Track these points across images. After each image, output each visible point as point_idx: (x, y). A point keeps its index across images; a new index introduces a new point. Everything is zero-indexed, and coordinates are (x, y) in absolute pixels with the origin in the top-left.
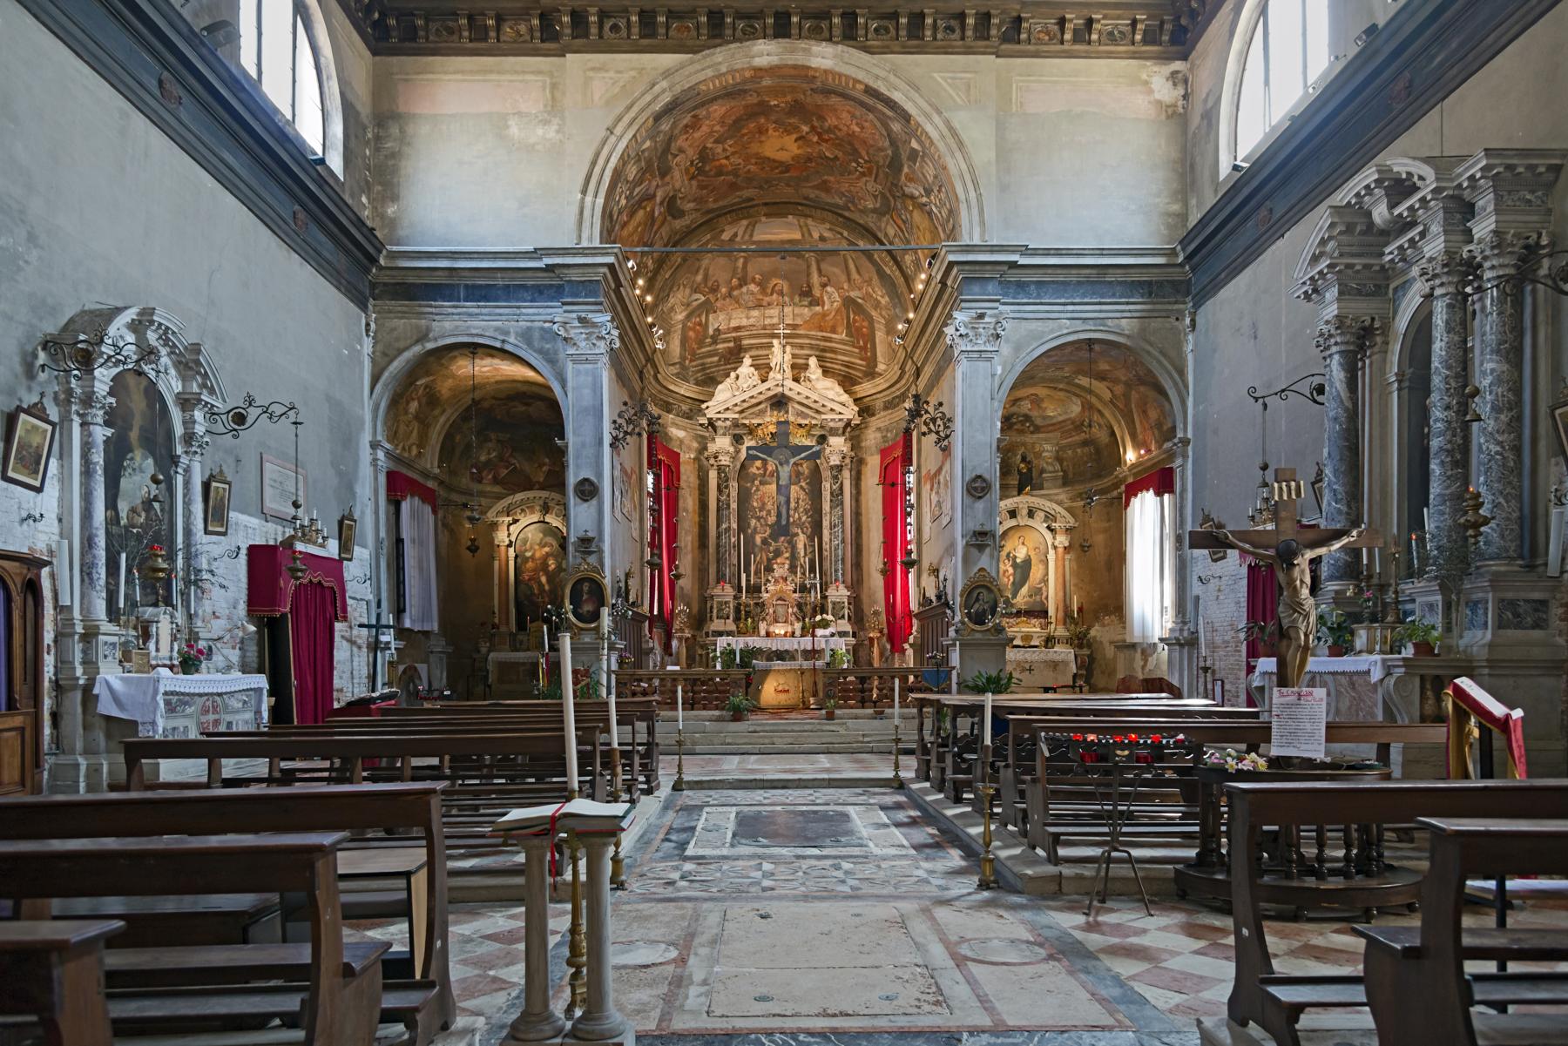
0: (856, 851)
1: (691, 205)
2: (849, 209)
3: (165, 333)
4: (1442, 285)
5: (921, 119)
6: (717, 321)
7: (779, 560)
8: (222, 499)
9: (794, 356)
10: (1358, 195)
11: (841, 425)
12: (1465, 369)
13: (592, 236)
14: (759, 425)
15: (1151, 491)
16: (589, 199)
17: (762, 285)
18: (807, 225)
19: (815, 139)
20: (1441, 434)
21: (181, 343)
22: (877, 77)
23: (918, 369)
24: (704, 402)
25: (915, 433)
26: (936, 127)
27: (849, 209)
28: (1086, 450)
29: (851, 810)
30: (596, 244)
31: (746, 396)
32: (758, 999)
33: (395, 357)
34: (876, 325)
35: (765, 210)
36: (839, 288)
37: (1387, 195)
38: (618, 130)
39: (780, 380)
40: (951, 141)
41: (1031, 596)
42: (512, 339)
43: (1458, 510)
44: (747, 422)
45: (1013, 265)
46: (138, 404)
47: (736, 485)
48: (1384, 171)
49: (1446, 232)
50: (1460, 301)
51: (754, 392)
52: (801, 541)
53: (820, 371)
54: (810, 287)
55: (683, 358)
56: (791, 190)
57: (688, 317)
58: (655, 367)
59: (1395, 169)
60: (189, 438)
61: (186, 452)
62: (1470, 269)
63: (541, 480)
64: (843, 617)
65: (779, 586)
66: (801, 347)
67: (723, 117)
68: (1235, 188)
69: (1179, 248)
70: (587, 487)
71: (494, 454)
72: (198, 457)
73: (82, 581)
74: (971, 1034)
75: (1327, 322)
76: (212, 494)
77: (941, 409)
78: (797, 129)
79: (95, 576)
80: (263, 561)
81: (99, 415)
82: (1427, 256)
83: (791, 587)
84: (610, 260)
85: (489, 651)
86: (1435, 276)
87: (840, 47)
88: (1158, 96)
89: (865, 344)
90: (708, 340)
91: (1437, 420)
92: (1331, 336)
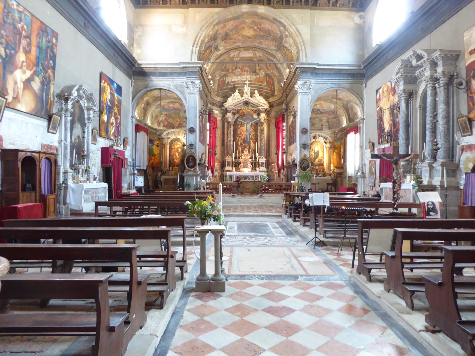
0: (271, 235)
1: (222, 48)
2: (267, 49)
3: (85, 91)
4: (429, 84)
5: (289, 27)
6: (229, 79)
7: (245, 149)
8: (96, 135)
9: (251, 90)
10: (408, 57)
11: (264, 110)
12: (435, 107)
13: (195, 59)
14: (240, 110)
15: (353, 132)
16: (194, 48)
17: (242, 69)
18: (255, 53)
19: (259, 30)
20: (429, 124)
21: (88, 93)
22: (277, 15)
23: (287, 95)
24: (224, 103)
25: (286, 115)
26: (293, 29)
27: (267, 49)
28: (335, 119)
29: (268, 223)
30: (196, 61)
31: (236, 101)
32: (250, 268)
33: (139, 92)
34: (275, 81)
35: (243, 49)
36: (264, 71)
37: (416, 58)
38: (203, 29)
39: (247, 97)
40: (297, 33)
41: (319, 162)
42: (172, 87)
43: (433, 145)
44: (236, 109)
45: (315, 68)
46: (77, 110)
47: (233, 127)
48: (415, 52)
49: (430, 70)
50: (434, 88)
51: (239, 100)
52: (252, 143)
53: (258, 94)
54: (256, 70)
55: (218, 90)
56: (251, 44)
57: (220, 78)
58: (210, 93)
59: (417, 52)
60: (89, 118)
61: (88, 122)
62: (436, 80)
63: (177, 126)
64: (264, 166)
65: (246, 157)
66: (253, 87)
67: (232, 25)
68: (377, 50)
69: (362, 65)
70: (192, 129)
71: (164, 118)
72: (91, 124)
73: (64, 158)
74: (301, 276)
75: (401, 91)
76: (93, 133)
77: (294, 108)
78: (253, 27)
79: (67, 157)
80: (105, 152)
81: (69, 114)
82: (426, 76)
83: (249, 157)
84: (200, 65)
85: (161, 175)
86: (428, 81)
87: (266, 7)
88: (356, 22)
89: (272, 86)
90: (226, 85)
91: (428, 120)
92: (401, 94)
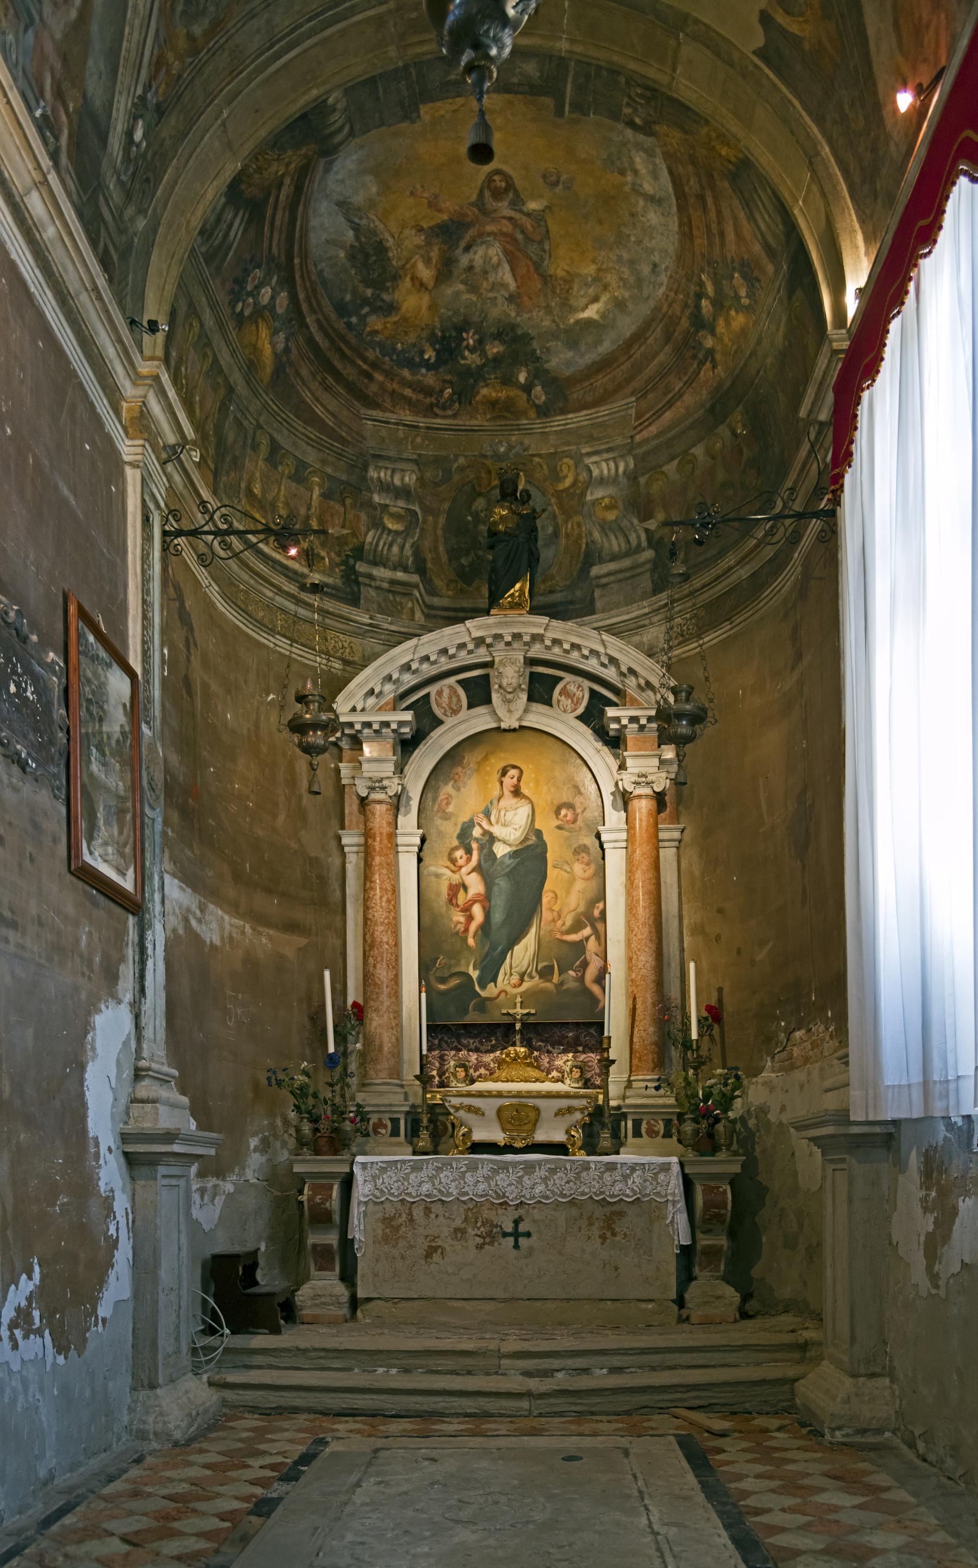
41: (545, 973)
